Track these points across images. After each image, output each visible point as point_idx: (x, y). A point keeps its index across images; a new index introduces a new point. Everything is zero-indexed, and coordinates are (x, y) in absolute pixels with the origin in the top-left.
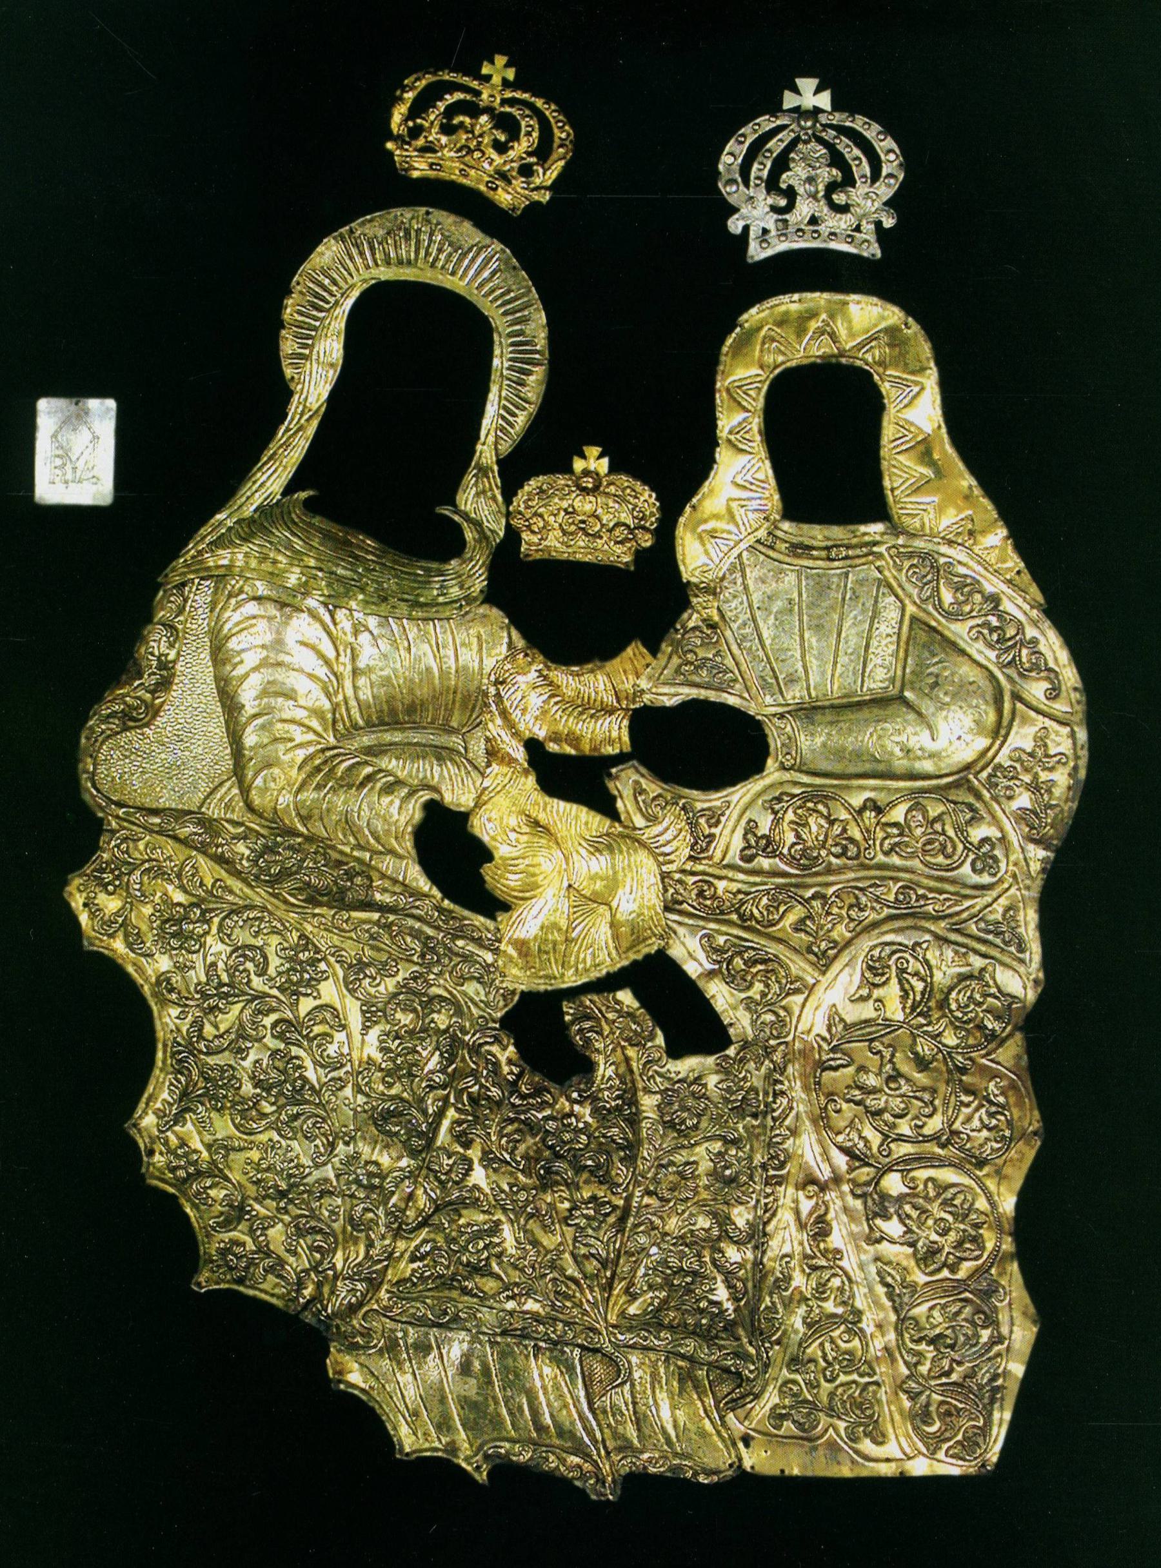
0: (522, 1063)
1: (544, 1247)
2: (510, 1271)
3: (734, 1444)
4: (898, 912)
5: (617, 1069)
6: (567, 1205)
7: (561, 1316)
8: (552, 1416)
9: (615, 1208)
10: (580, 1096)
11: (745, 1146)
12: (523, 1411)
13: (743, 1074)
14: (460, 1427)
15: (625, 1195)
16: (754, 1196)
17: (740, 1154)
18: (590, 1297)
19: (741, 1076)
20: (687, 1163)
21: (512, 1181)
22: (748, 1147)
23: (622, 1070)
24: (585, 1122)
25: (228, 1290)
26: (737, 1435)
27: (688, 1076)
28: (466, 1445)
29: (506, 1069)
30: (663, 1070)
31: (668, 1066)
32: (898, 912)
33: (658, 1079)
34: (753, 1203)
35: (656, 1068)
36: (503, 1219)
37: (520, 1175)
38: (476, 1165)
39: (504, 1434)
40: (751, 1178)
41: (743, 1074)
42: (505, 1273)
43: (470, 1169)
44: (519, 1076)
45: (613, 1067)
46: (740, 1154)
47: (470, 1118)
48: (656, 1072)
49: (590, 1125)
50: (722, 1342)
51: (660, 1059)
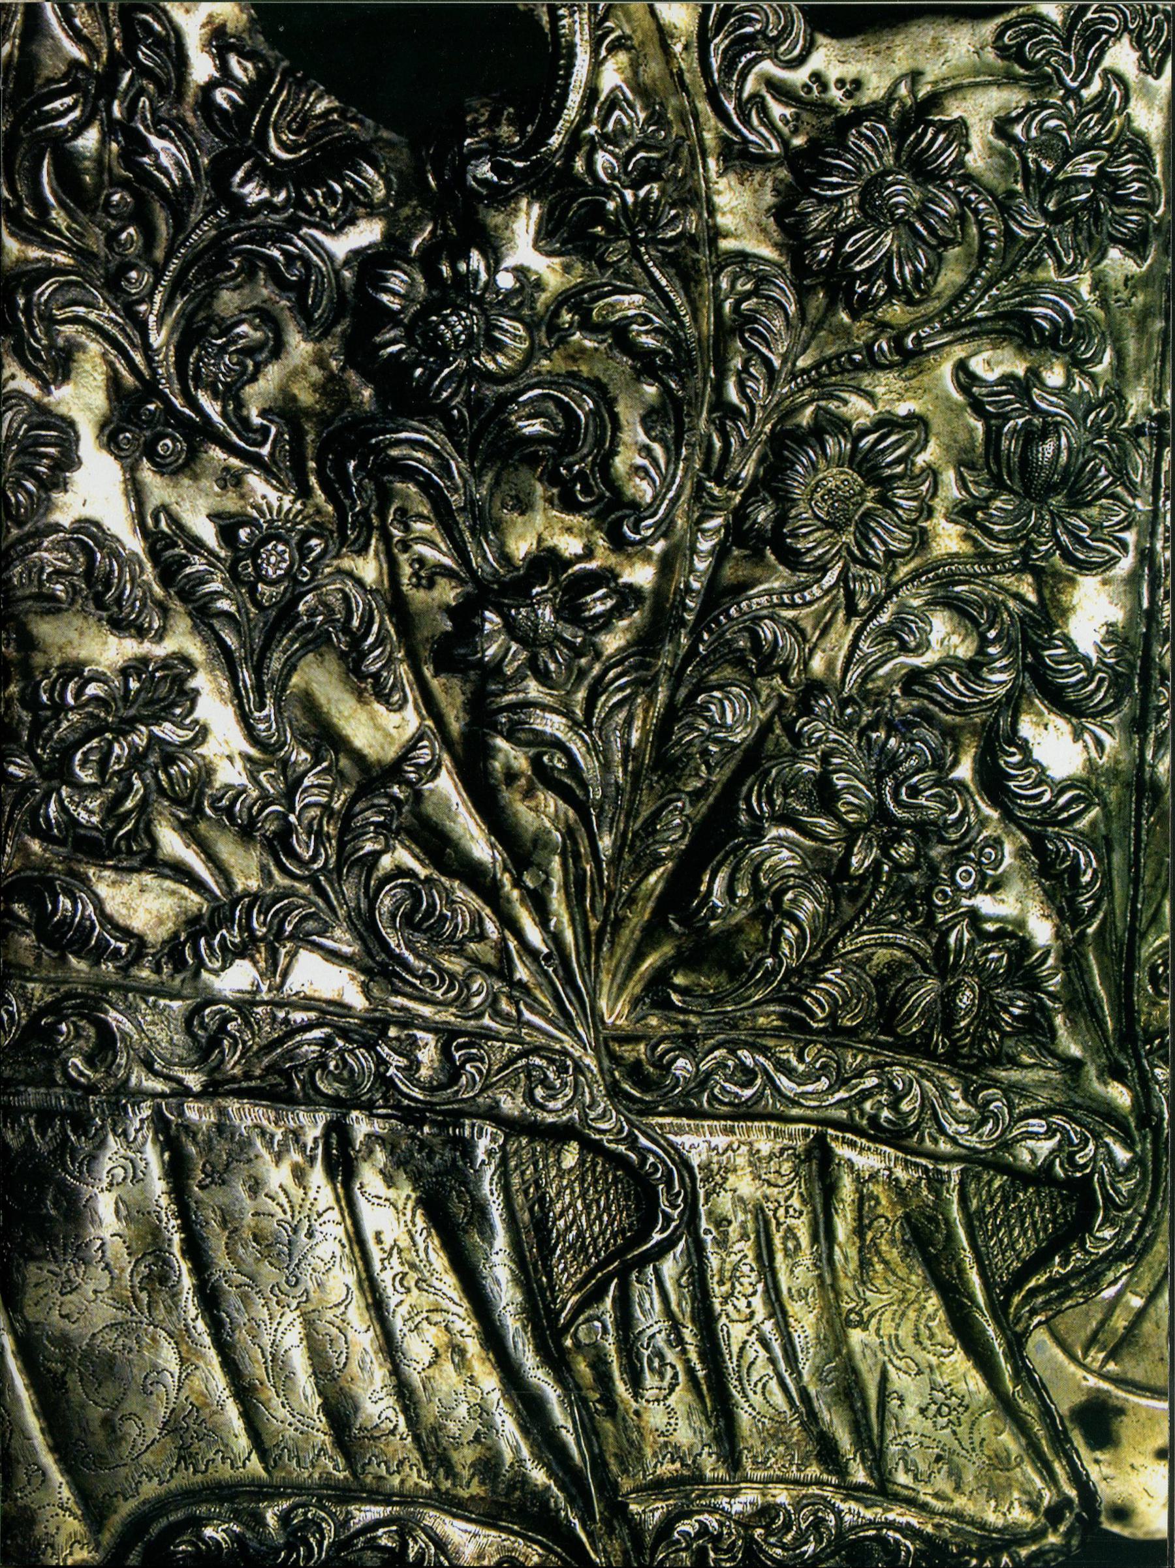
0: (260, 42)
1: (358, 757)
2: (228, 849)
3: (1060, 1440)
4: (1118, 1286)
5: (635, 65)
6: (448, 593)
7: (426, 1011)
8: (403, 1391)
9: (629, 596)
10: (499, 169)
11: (1096, 359)
12: (290, 1377)
13: (1096, 86)
14: (48, 1460)
15: (658, 547)
16: (1130, 537)
17: (1081, 385)
18: (534, 936)
19: (1087, 94)
20: (887, 423)
21: (231, 503)
22: (1108, 357)
23: (653, 69)
24: (520, 272)
25: (569, 787)
26: (1064, 1403)
27: (891, 96)
28: (73, 1525)
29: (202, 68)
30: (799, 76)
31: (817, 61)
32: (1118, 1286)
33: (777, 110)
34: (1126, 564)
35: (767, 66)
36: (196, 650)
37: (256, 483)
38: (89, 446)
39: (225, 1472)
40: (1121, 473)
41: (1096, 86)
42: (212, 858)
43: (68, 461)
44: (255, 93)
45: (622, 57)
46: (1081, 385)
47: (62, 258)
48: (771, 84)
49: (539, 285)
50: (1015, 1075)
51: (785, 32)
